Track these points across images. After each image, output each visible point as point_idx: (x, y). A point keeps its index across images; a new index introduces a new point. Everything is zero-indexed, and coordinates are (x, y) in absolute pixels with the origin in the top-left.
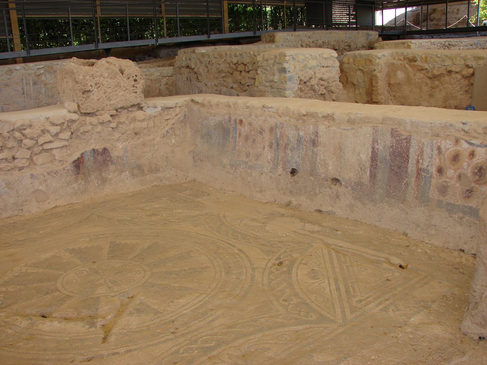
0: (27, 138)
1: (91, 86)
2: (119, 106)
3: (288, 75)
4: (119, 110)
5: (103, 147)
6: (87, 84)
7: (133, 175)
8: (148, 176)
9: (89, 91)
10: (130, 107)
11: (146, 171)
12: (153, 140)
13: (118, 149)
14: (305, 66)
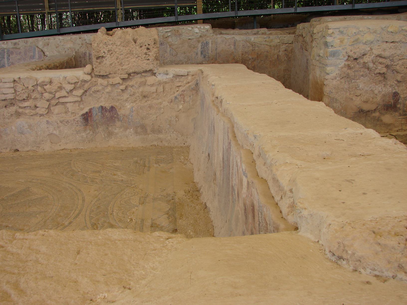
0: (47, 92)
1: (104, 52)
2: (131, 71)
3: (330, 49)
4: (132, 75)
5: (110, 105)
6: (100, 51)
7: (136, 133)
8: (150, 136)
9: (103, 57)
10: (142, 73)
11: (149, 131)
12: (161, 103)
13: (127, 108)
14: (357, 41)
